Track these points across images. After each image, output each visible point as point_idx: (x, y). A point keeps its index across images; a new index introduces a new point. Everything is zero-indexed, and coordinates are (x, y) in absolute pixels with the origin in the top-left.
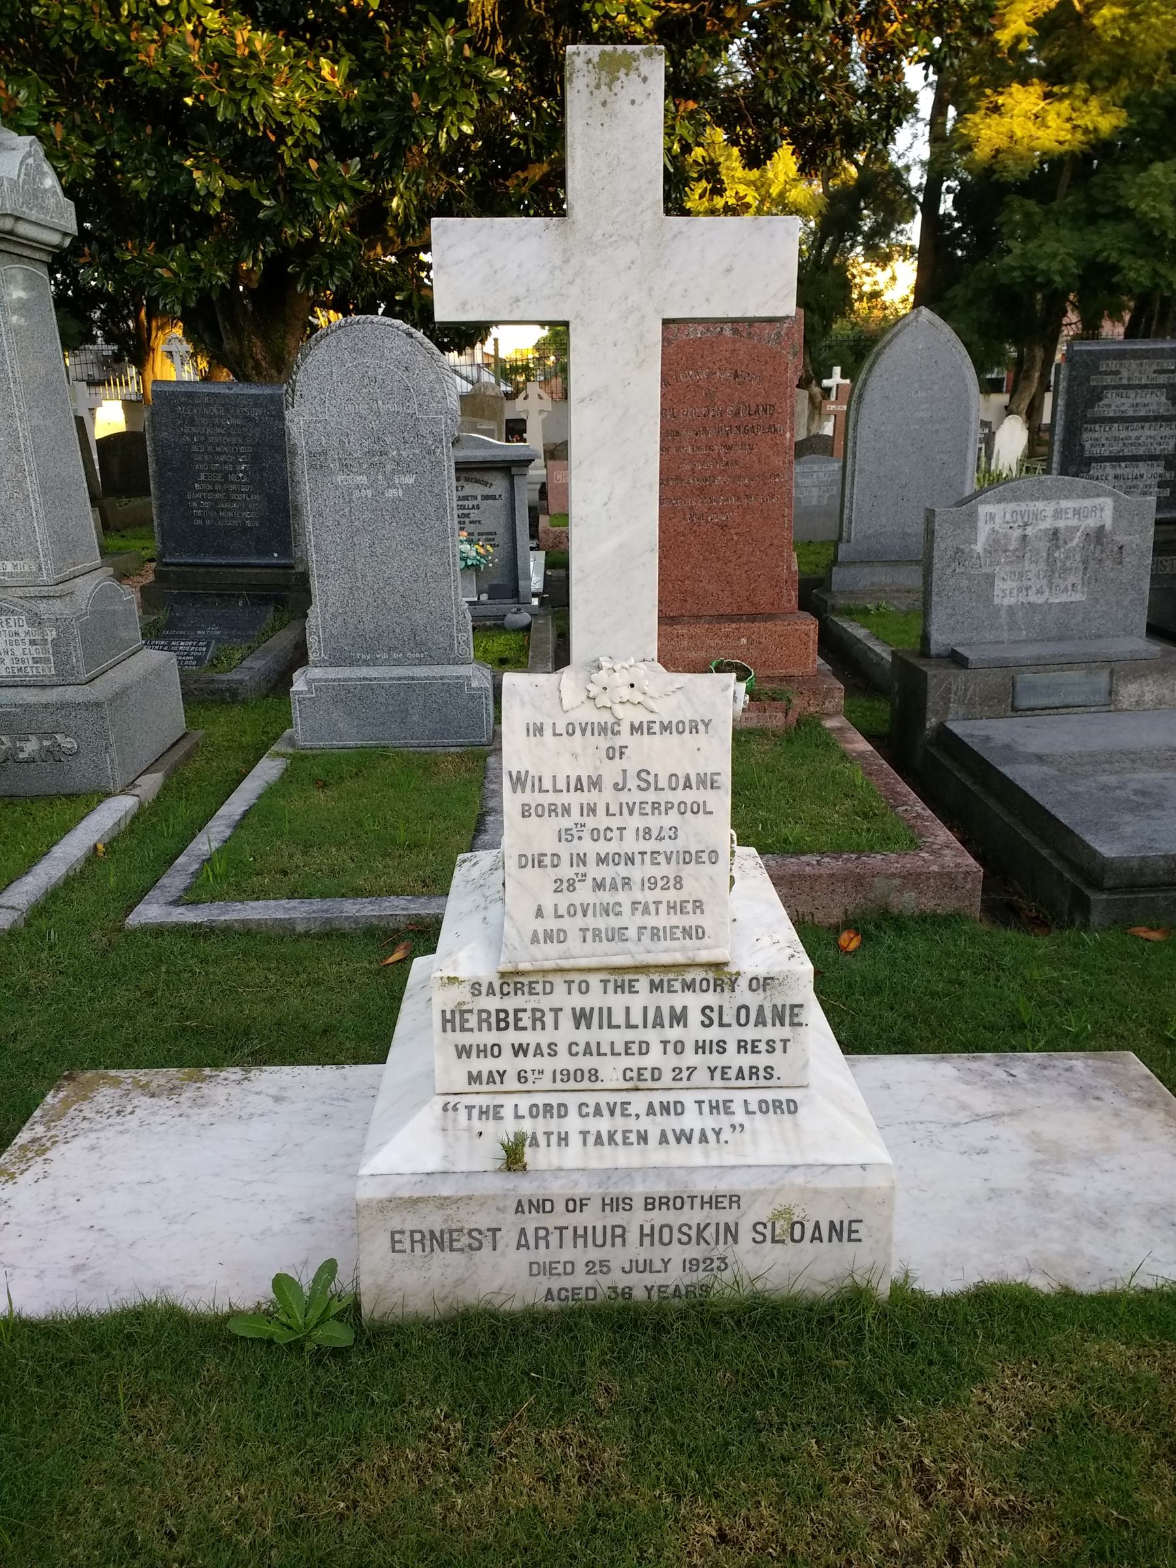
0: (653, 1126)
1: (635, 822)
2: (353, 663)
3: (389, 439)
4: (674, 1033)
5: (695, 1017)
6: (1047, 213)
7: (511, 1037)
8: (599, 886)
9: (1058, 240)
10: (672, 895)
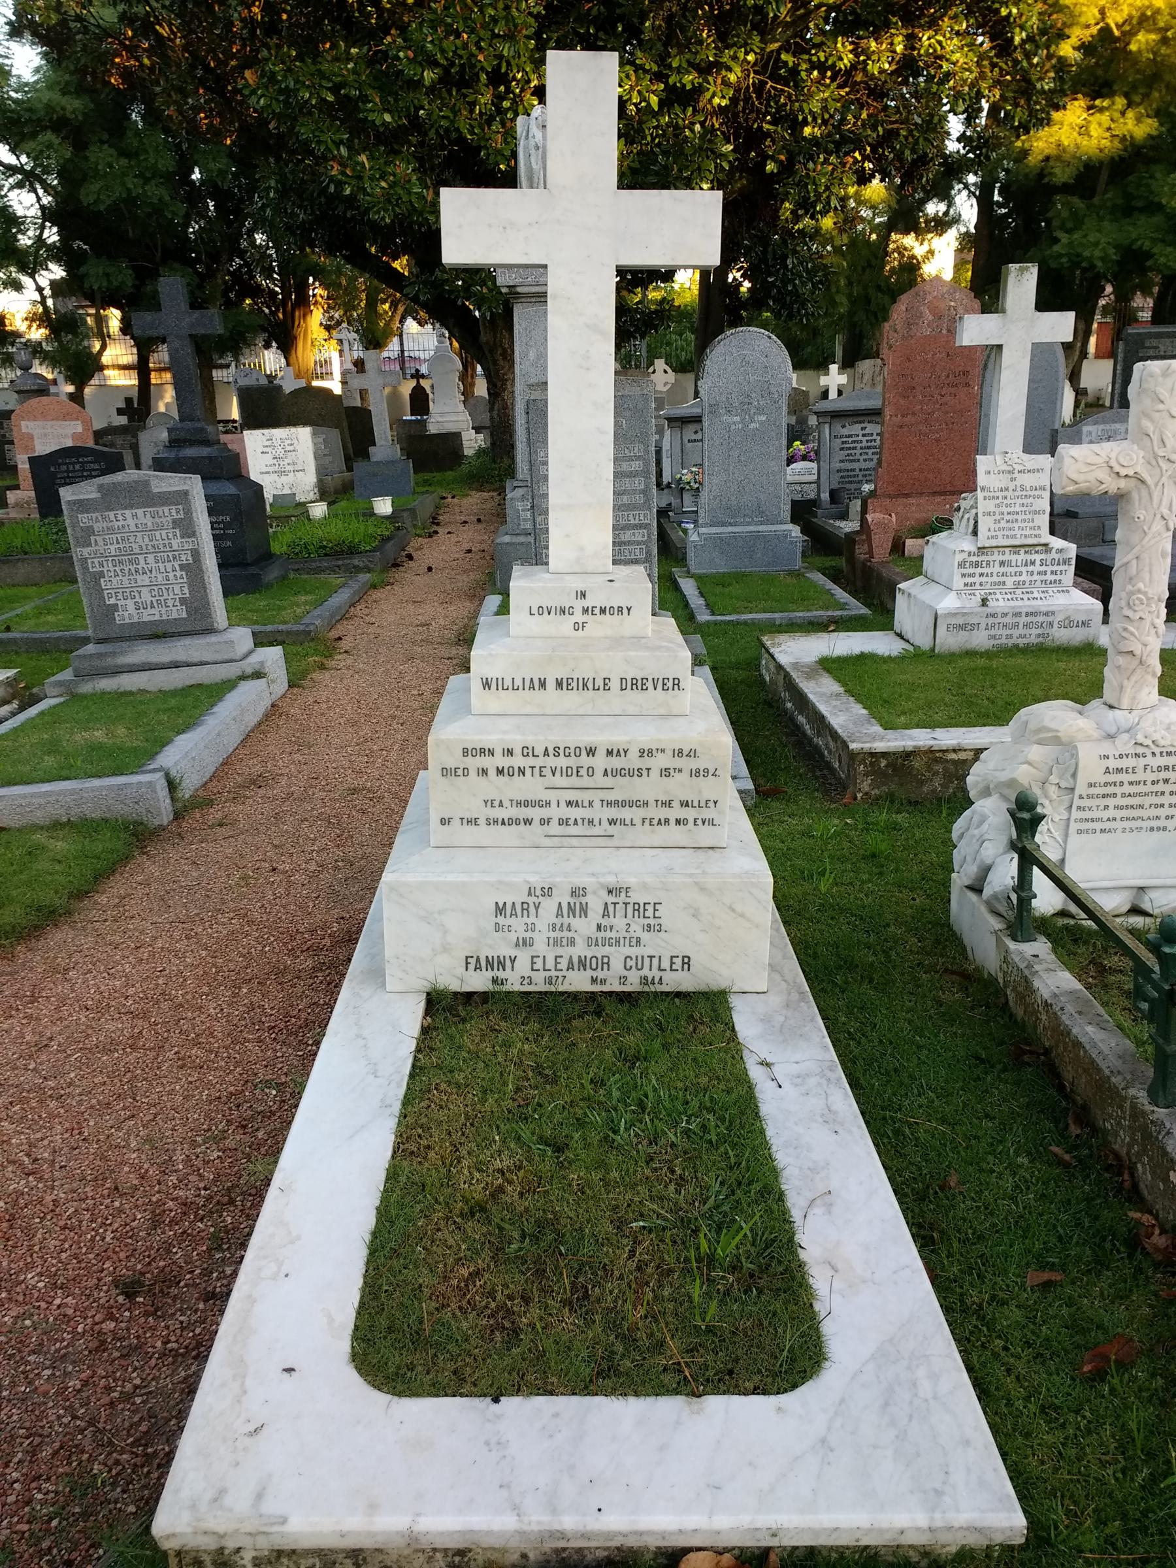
0: (1025, 596)
1: (1019, 501)
2: (723, 524)
3: (753, 395)
4: (1031, 568)
5: (1038, 563)
6: (1088, 207)
7: (979, 570)
8: (1008, 521)
9: (1099, 231)
10: (1031, 524)
